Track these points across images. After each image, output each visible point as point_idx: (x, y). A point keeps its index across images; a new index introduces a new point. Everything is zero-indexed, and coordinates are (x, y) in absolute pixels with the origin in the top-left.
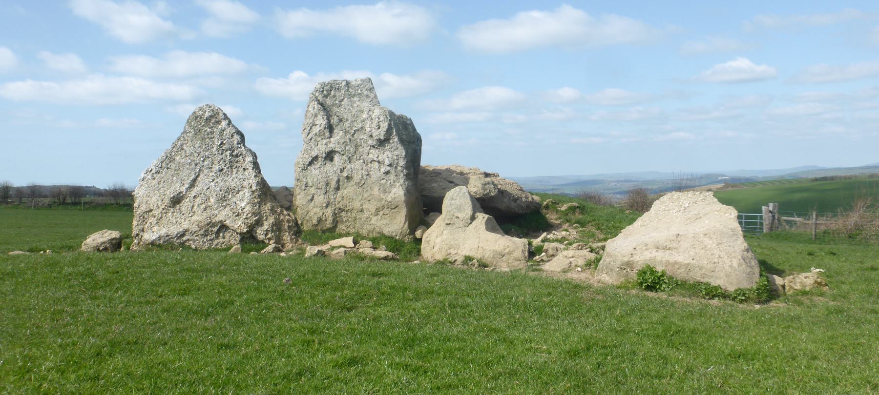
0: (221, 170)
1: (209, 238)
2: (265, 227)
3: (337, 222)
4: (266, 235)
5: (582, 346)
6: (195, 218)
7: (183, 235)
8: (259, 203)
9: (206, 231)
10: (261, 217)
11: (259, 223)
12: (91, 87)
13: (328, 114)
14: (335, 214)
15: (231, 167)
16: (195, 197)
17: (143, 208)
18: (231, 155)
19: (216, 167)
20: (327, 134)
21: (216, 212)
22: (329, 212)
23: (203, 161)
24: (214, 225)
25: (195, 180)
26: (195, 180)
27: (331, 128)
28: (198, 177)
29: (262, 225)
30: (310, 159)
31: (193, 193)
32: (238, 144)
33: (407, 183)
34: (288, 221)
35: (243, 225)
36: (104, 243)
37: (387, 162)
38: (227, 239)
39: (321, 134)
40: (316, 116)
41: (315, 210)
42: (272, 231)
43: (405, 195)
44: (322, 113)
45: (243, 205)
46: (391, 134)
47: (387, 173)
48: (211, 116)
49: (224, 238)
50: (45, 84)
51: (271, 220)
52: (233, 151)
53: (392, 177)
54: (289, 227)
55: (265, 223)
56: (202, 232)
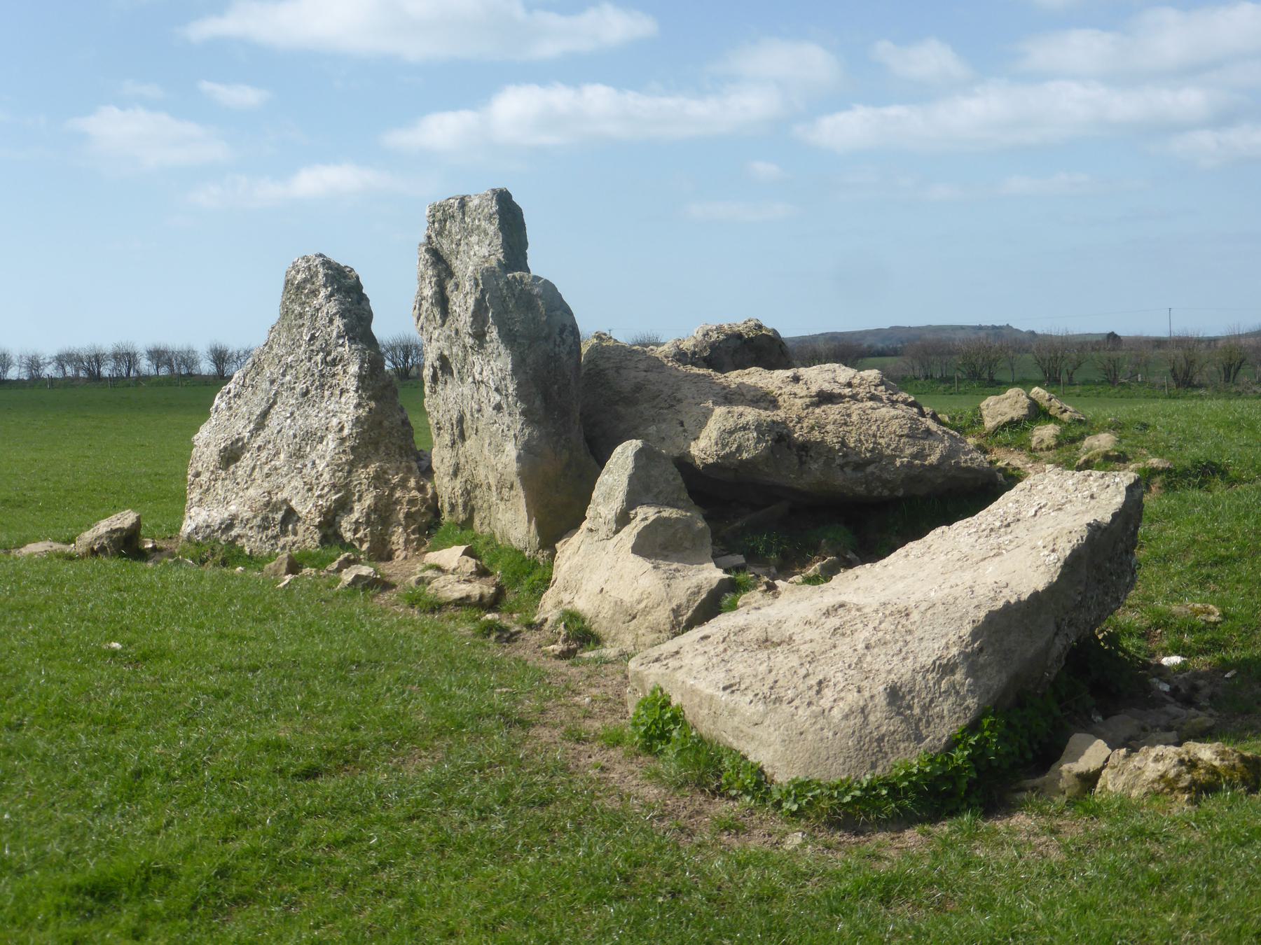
1: (270, 532)
2: (355, 515)
3: (473, 510)
4: (356, 531)
5: (16, 865)
7: (230, 526)
8: (352, 464)
9: (265, 519)
10: (349, 494)
11: (344, 506)
12: (979, 110)
15: (322, 386)
16: (259, 447)
18: (324, 361)
19: (300, 387)
21: (285, 480)
23: (284, 375)
24: (276, 508)
25: (265, 414)
26: (265, 414)
28: (271, 407)
29: (351, 510)
31: (259, 441)
32: (339, 337)
33: (527, 431)
34: (412, 502)
36: (100, 537)
38: (299, 538)
42: (368, 523)
43: (519, 458)
46: (485, 322)
48: (305, 281)
49: (295, 534)
50: (894, 111)
51: (368, 500)
52: (329, 354)
54: (408, 516)
55: (357, 507)
56: (258, 521)
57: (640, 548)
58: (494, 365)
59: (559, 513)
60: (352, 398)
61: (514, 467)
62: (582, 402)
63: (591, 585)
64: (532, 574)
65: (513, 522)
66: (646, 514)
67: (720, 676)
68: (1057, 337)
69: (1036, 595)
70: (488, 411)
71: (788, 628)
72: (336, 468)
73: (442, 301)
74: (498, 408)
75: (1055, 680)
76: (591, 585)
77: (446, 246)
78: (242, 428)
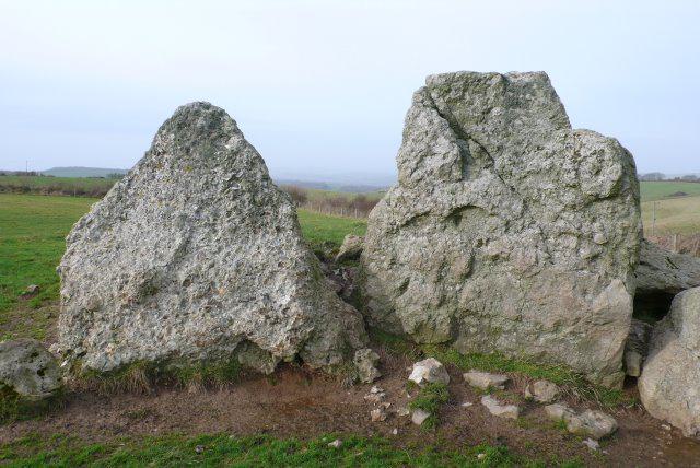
0: (234, 230)
6: (189, 326)
11: (314, 337)
13: (459, 133)
14: (453, 319)
17: (83, 301)
18: (253, 202)
20: (457, 174)
22: (443, 314)
27: (464, 161)
30: (409, 216)
35: (287, 345)
37: (598, 237)
39: (444, 172)
40: (435, 137)
41: (412, 308)
44: (448, 132)
45: (285, 300)
47: (595, 257)
53: (603, 266)
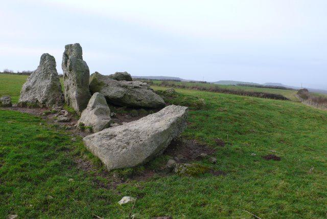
11: (47, 100)
51: (51, 99)
57: (96, 113)
58: (73, 76)
59: (83, 106)
60: (50, 81)
61: (75, 96)
62: (90, 85)
63: (87, 118)
64: (75, 115)
65: (75, 106)
66: (98, 106)
67: (99, 143)
68: (213, 84)
69: (165, 131)
70: (72, 85)
71: (116, 133)
72: (46, 92)
73: (66, 63)
74: (73, 84)
75: (171, 145)
76: (87, 118)
77: (68, 53)
78: (30, 84)
